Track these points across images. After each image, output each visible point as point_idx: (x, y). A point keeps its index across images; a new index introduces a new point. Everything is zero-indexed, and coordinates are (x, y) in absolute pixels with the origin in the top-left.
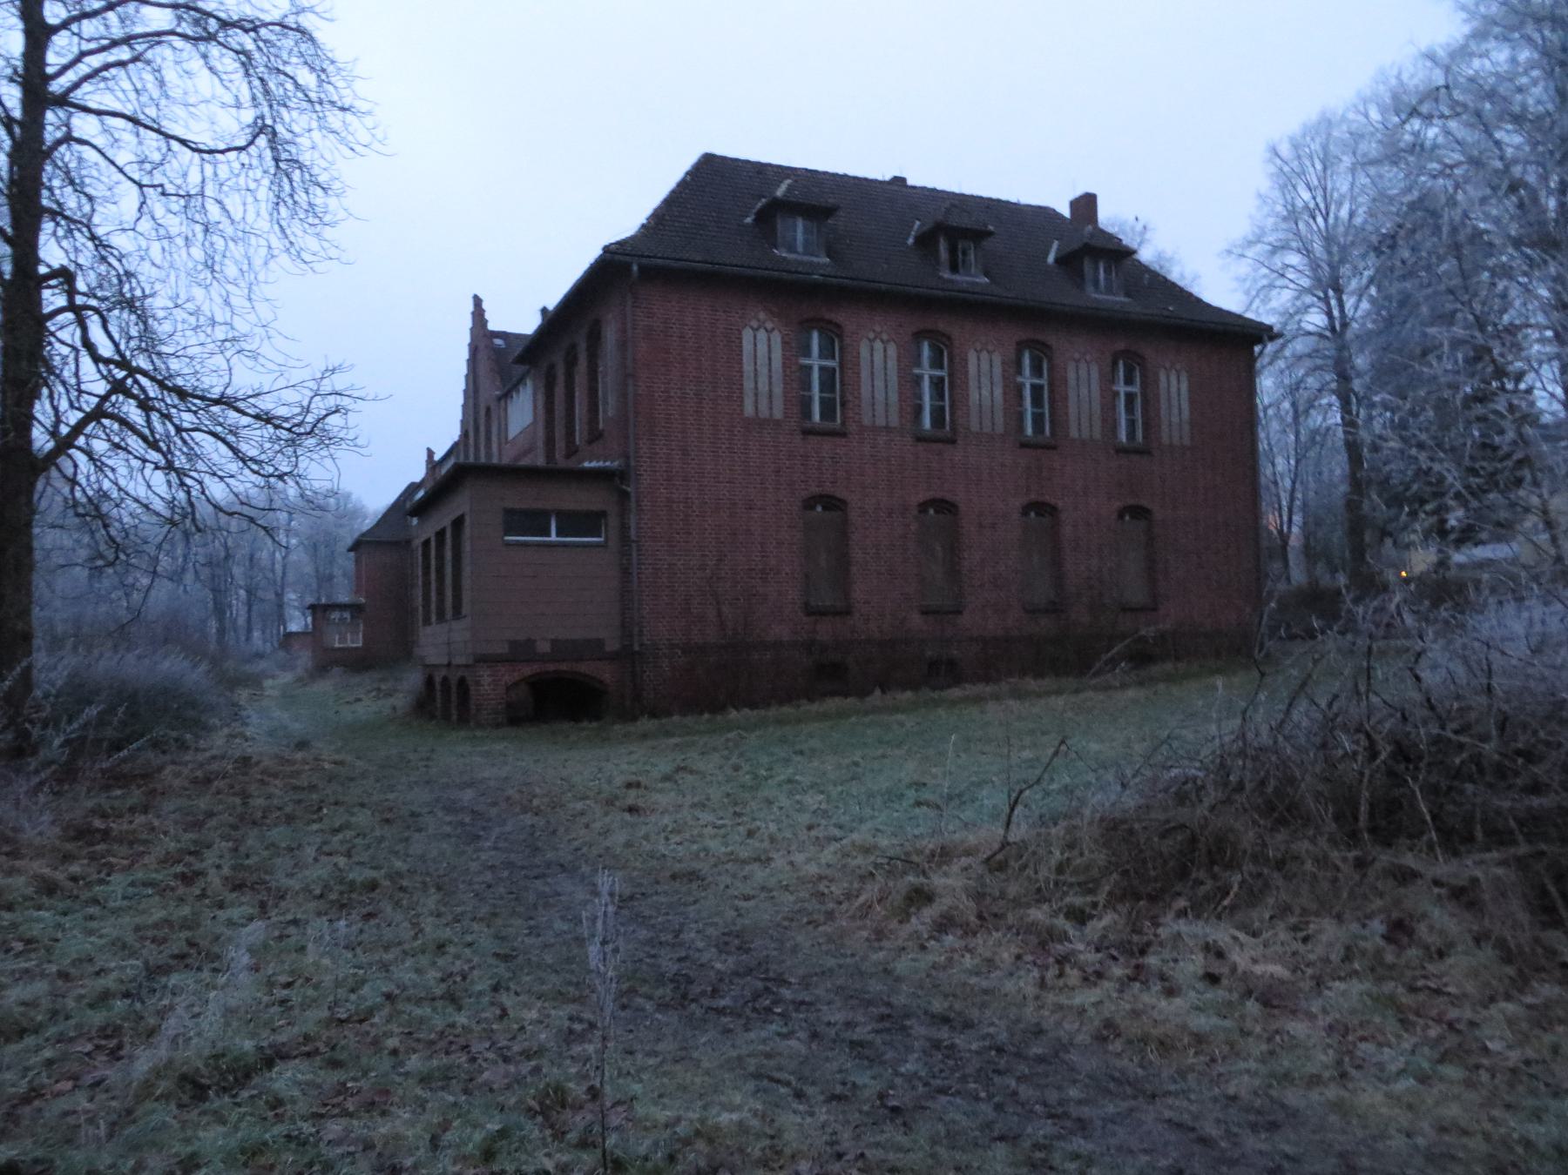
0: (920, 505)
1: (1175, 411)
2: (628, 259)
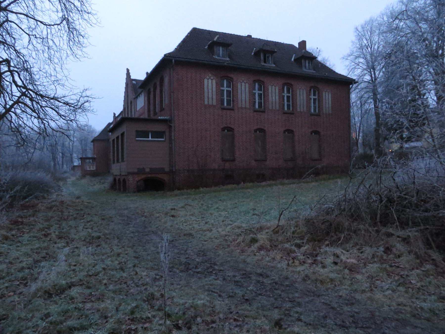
1: (327, 104)
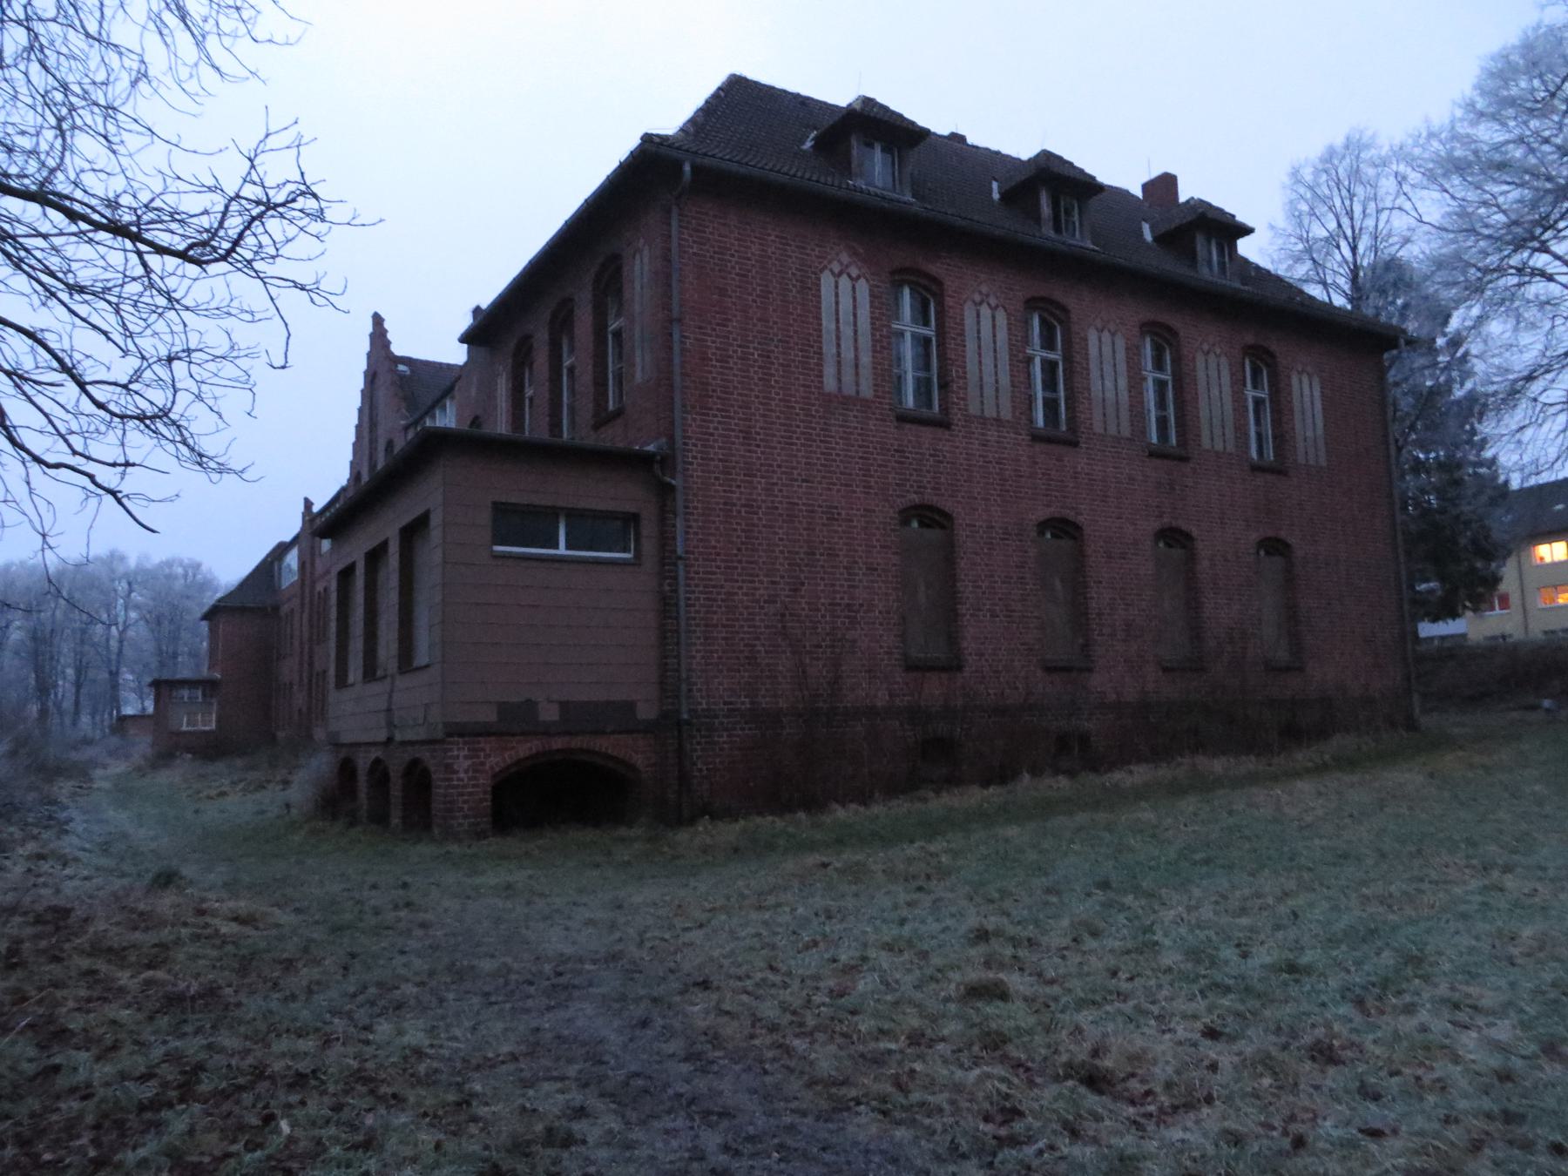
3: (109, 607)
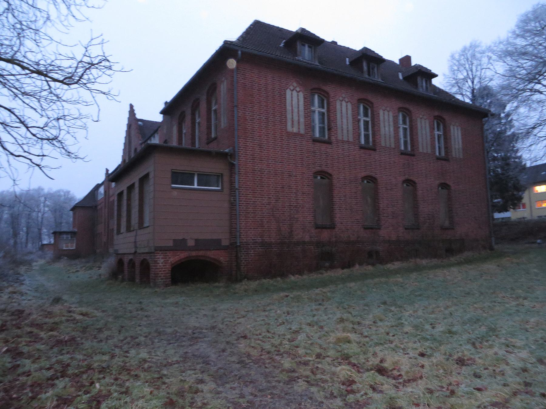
0: (362, 178)
2: (236, 48)
3: (38, 206)
